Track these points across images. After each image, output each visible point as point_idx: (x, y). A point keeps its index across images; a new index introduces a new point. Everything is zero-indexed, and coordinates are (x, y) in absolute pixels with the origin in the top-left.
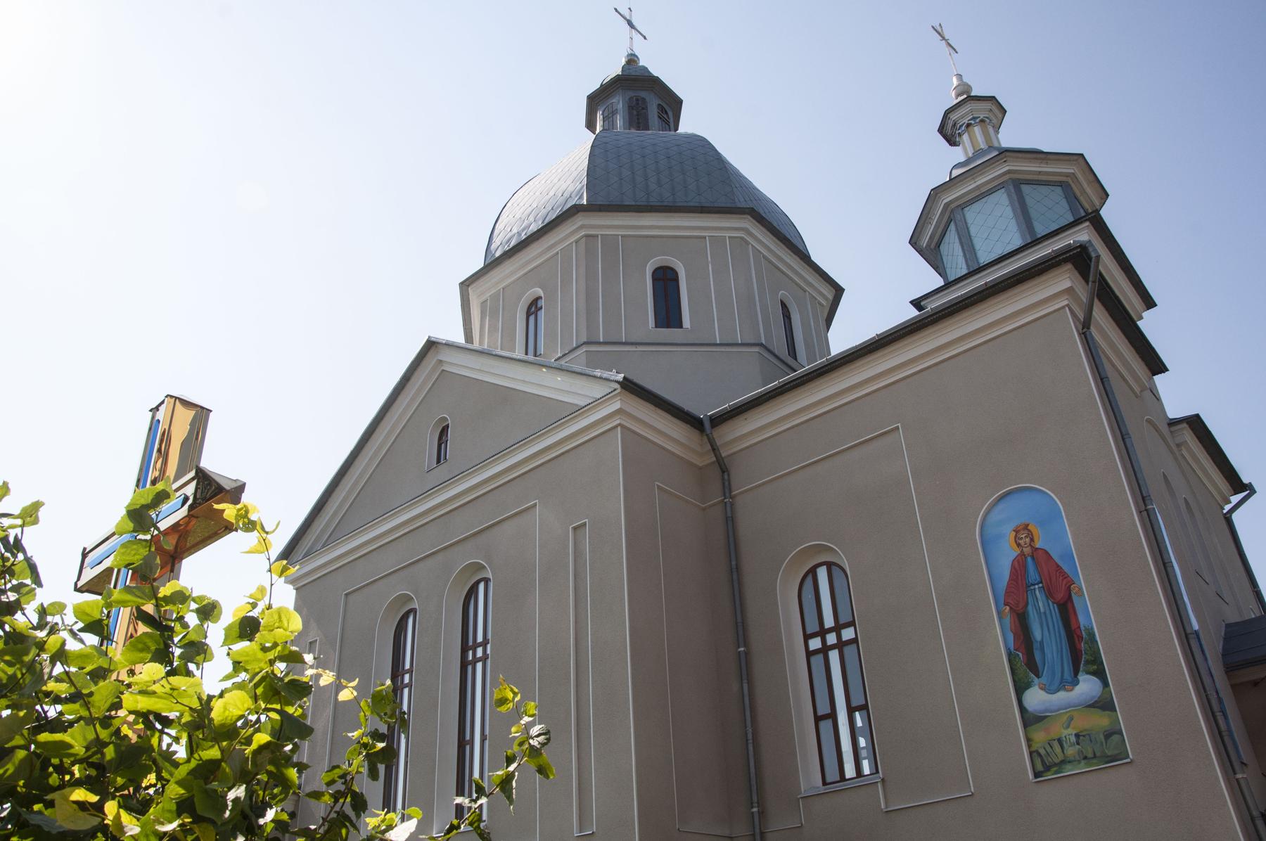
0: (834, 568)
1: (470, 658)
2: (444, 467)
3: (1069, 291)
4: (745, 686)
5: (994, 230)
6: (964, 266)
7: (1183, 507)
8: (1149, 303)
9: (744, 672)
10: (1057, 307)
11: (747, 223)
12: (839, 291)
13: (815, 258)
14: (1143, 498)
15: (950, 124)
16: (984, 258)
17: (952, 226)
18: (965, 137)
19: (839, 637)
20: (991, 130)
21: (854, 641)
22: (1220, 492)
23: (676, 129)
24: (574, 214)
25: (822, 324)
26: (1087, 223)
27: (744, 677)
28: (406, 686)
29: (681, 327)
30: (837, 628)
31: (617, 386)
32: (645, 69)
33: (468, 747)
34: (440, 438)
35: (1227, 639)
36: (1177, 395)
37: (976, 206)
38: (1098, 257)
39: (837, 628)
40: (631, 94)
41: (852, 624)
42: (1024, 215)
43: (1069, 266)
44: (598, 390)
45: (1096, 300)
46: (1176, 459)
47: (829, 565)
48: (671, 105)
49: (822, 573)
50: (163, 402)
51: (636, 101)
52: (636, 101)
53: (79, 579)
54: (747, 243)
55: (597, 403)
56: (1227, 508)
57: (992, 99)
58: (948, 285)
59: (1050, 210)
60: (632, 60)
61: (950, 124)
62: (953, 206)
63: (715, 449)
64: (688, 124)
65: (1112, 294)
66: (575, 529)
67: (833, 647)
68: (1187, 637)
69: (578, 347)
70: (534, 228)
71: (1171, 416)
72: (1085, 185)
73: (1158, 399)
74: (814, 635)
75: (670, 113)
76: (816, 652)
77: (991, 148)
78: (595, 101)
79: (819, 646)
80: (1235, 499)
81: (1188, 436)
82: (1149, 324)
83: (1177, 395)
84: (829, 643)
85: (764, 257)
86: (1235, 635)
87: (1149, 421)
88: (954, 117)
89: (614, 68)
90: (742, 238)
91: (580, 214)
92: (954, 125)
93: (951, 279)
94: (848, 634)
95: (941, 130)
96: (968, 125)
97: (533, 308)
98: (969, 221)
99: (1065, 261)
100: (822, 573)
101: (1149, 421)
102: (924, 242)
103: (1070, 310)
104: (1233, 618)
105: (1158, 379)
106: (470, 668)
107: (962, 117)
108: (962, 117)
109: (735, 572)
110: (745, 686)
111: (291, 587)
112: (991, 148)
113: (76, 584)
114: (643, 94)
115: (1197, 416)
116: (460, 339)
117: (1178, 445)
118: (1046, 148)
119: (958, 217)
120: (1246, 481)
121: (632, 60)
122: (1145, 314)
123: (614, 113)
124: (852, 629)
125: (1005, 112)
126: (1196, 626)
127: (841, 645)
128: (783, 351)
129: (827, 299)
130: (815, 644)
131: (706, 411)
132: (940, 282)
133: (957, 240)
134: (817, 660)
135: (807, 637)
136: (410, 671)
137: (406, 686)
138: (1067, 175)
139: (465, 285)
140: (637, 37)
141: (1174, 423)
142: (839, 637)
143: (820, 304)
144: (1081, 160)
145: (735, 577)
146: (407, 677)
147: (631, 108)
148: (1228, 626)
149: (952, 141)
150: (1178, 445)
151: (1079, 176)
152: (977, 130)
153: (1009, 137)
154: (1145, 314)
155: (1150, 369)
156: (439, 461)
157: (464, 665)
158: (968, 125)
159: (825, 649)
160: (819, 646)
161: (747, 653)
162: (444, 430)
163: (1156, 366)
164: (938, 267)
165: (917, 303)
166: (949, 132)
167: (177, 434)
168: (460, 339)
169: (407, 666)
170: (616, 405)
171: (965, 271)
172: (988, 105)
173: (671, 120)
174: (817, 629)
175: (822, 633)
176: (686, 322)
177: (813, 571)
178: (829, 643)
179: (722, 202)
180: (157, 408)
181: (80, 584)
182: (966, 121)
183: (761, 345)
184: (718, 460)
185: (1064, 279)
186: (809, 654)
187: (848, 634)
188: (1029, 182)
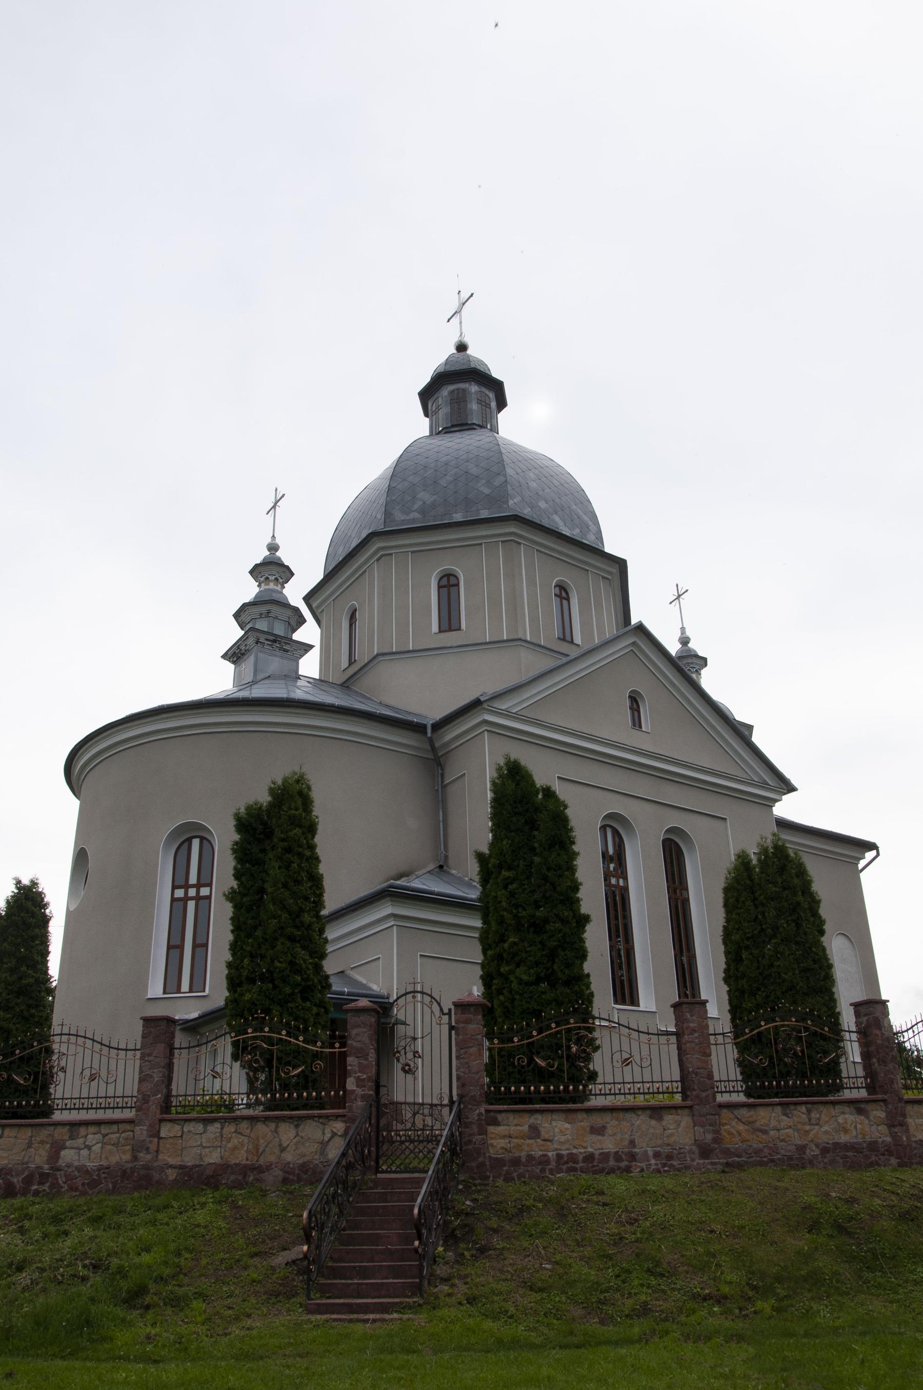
0: (205, 841)
19: (198, 892)
21: (209, 898)
24: (372, 538)
30: (198, 886)
39: (198, 886)
47: (202, 839)
49: (196, 843)
67: (192, 898)
71: (233, 666)
74: (179, 887)
76: (179, 899)
78: (426, 395)
91: (375, 538)
94: (204, 891)
100: (196, 843)
114: (462, 386)
124: (176, 896)
125: (621, 565)
127: (198, 898)
130: (179, 893)
135: (174, 888)
142: (198, 892)
159: (186, 899)
175: (187, 886)
176: (463, 626)
177: (189, 840)
181: (874, 853)
186: (173, 900)
187: (204, 891)
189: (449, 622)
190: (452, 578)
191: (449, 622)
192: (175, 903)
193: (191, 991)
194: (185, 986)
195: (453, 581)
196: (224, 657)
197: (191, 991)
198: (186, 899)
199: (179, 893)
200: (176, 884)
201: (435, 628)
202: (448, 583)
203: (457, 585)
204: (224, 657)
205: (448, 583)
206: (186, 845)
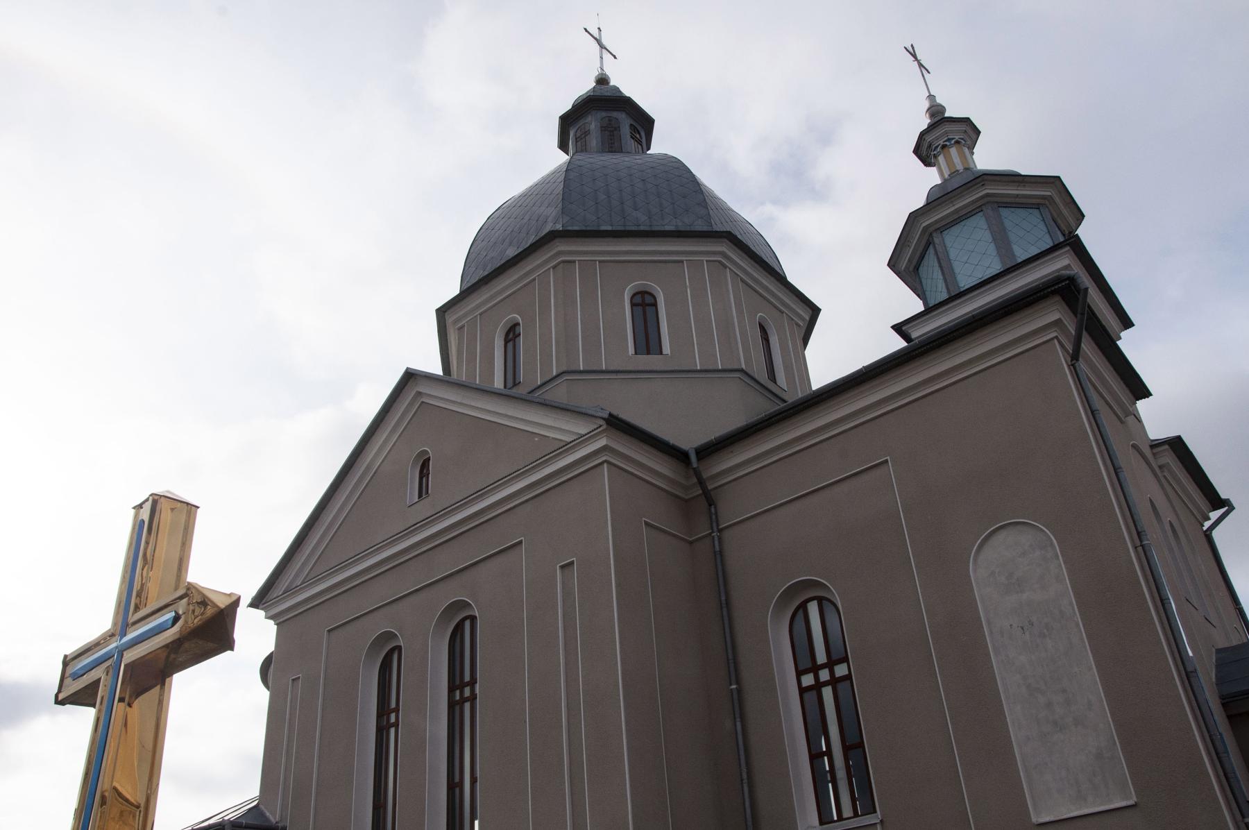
1: (458, 698)
2: (426, 502)
3: (1058, 323)
4: (739, 724)
5: (972, 254)
6: (945, 290)
7: (1168, 527)
8: (1127, 323)
9: (737, 709)
10: (1045, 339)
11: (723, 247)
12: (815, 311)
13: (791, 279)
14: (1139, 533)
15: (926, 145)
16: (965, 282)
17: (931, 250)
18: (941, 159)
20: (966, 150)
21: (848, 677)
22: (1198, 508)
23: (649, 149)
25: (799, 343)
26: (1068, 248)
27: (737, 715)
28: (392, 725)
29: (661, 353)
30: (830, 665)
31: (602, 422)
32: (616, 89)
33: (457, 790)
34: (421, 472)
35: (1219, 666)
36: (1156, 418)
37: (955, 230)
38: (1086, 289)
39: (830, 665)
40: (604, 114)
41: (845, 659)
42: (1002, 241)
43: (1057, 298)
44: (582, 428)
45: (1085, 335)
46: (1159, 481)
47: (820, 600)
48: (643, 124)
49: (813, 609)
50: (147, 500)
51: (605, 120)
52: (605, 120)
53: (60, 691)
54: (725, 267)
55: (582, 440)
56: (1207, 524)
57: (967, 121)
58: (929, 310)
59: (1029, 235)
60: (602, 80)
61: (926, 145)
62: (932, 229)
63: (701, 482)
64: (659, 146)
65: (1085, 310)
66: (562, 567)
67: (826, 684)
68: (1189, 676)
69: (557, 376)
70: (511, 252)
71: (1152, 437)
72: (1062, 206)
73: (1140, 421)
74: (806, 672)
75: (643, 134)
76: (809, 688)
77: (967, 169)
78: (567, 121)
79: (813, 682)
80: (1214, 515)
81: (1169, 458)
82: (1128, 343)
83: (1156, 418)
84: (822, 679)
85: (742, 280)
86: (1228, 659)
87: (1134, 446)
88: (929, 138)
89: (586, 85)
90: (720, 262)
91: (557, 240)
92: (930, 146)
93: (932, 303)
94: (841, 670)
95: (917, 151)
96: (944, 147)
97: (512, 334)
98: (948, 244)
99: (1053, 293)
100: (813, 609)
101: (1134, 446)
102: (903, 265)
103: (1060, 342)
104: (1222, 644)
105: (1141, 405)
106: (457, 708)
107: (937, 138)
108: (937, 138)
109: (725, 605)
110: (739, 724)
111: (272, 622)
112: (967, 169)
113: (57, 696)
114: (615, 114)
115: (1179, 438)
116: (436, 368)
117: (1160, 467)
118: (1024, 171)
119: (936, 240)
120: (1223, 496)
121: (602, 80)
122: (1123, 334)
123: (587, 133)
126: (1191, 654)
128: (763, 377)
129: (803, 319)
130: (808, 680)
131: (688, 441)
132: (917, 306)
133: (936, 264)
134: (811, 697)
135: (799, 674)
136: (397, 710)
137: (392, 725)
138: (1044, 197)
139: (442, 312)
140: (606, 56)
141: (1156, 445)
142: (832, 673)
143: (797, 324)
144: (1057, 182)
145: (725, 613)
146: (393, 716)
147: (603, 129)
148: (1218, 651)
149: (927, 162)
150: (1160, 467)
151: (1057, 200)
152: (953, 151)
153: (986, 157)
154: (1123, 334)
155: (1210, 502)
156: (420, 496)
157: (452, 705)
158: (944, 147)
159: (818, 686)
160: (813, 682)
161: (739, 691)
162: (425, 465)
163: (1141, 391)
164: (921, 294)
165: (898, 329)
166: (925, 151)
167: (162, 526)
168: (436, 368)
169: (393, 705)
170: (602, 442)
171: (945, 296)
172: (963, 127)
173: (644, 140)
174: (809, 665)
175: (815, 669)
176: (666, 349)
177: (803, 607)
178: (822, 679)
179: (700, 226)
180: (140, 506)
181: (61, 697)
182: (941, 142)
183: (742, 371)
184: (704, 493)
185: (1054, 312)
186: (803, 691)
187: (841, 670)
188: (1007, 205)
189: (648, 341)
190: (646, 296)
191: (648, 341)
192: (806, 696)
193: (856, 815)
194: (847, 812)
195: (648, 299)
196: (893, 327)
197: (856, 815)
198: (818, 686)
199: (808, 680)
200: (801, 668)
201: (631, 350)
202: (644, 303)
203: (655, 305)
204: (893, 327)
205: (644, 303)
206: (801, 612)
